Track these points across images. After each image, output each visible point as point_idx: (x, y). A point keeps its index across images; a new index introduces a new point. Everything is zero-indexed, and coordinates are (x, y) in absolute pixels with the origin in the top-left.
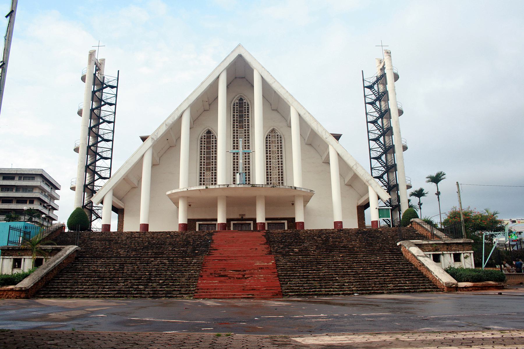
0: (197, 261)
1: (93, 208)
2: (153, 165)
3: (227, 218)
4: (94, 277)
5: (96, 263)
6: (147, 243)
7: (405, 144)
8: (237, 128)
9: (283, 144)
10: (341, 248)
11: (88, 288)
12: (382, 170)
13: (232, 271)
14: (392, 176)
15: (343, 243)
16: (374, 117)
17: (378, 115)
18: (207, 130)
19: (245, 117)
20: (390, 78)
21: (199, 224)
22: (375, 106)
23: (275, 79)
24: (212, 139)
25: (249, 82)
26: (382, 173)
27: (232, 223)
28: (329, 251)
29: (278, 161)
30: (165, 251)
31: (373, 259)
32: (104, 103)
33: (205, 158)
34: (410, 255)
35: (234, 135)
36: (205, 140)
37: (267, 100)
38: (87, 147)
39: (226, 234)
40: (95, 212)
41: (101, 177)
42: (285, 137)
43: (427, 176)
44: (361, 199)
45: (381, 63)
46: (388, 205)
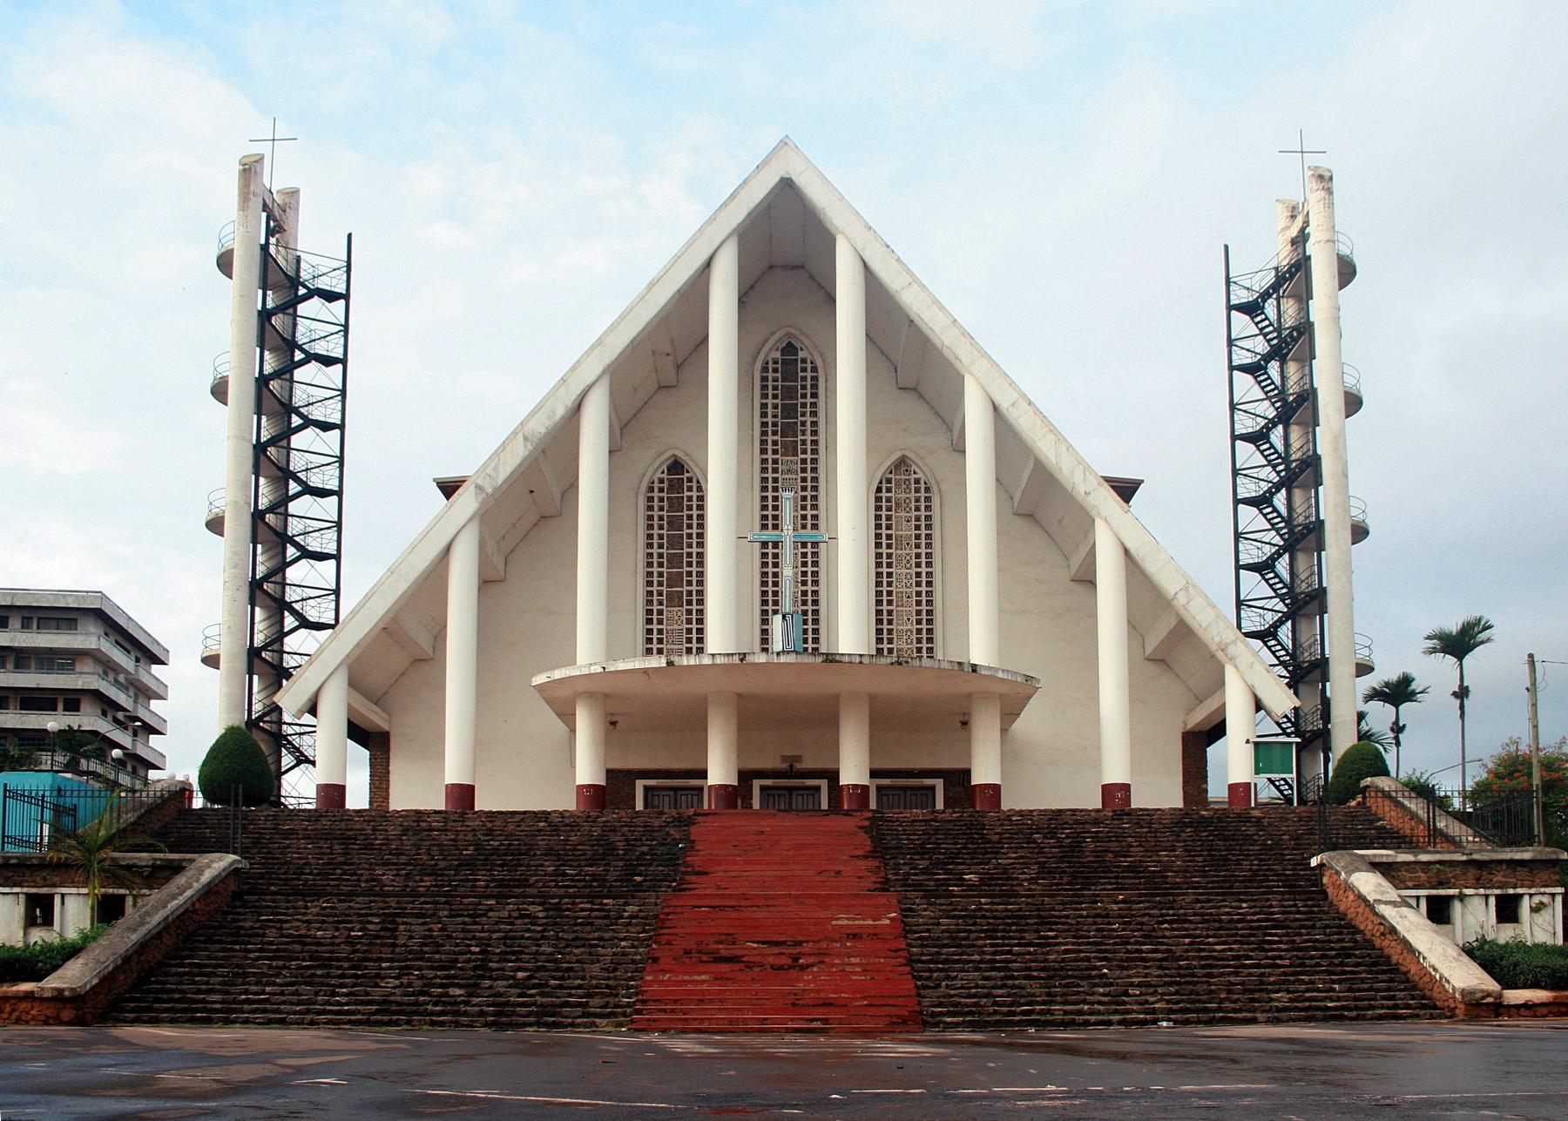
0: (640, 911)
1: (284, 727)
2: (485, 582)
5: (304, 914)
6: (472, 848)
7: (1361, 517)
8: (775, 452)
10: (1123, 872)
11: (282, 993)
12: (1273, 542)
14: (1308, 632)
16: (1259, 419)
17: (1271, 413)
18: (668, 459)
21: (647, 789)
23: (912, 274)
27: (757, 784)
29: (918, 575)
31: (1227, 910)
33: (665, 560)
35: (764, 480)
36: (665, 495)
39: (737, 823)
41: (305, 623)
42: (944, 487)
43: (1429, 632)
45: (1293, 217)
46: (1288, 731)
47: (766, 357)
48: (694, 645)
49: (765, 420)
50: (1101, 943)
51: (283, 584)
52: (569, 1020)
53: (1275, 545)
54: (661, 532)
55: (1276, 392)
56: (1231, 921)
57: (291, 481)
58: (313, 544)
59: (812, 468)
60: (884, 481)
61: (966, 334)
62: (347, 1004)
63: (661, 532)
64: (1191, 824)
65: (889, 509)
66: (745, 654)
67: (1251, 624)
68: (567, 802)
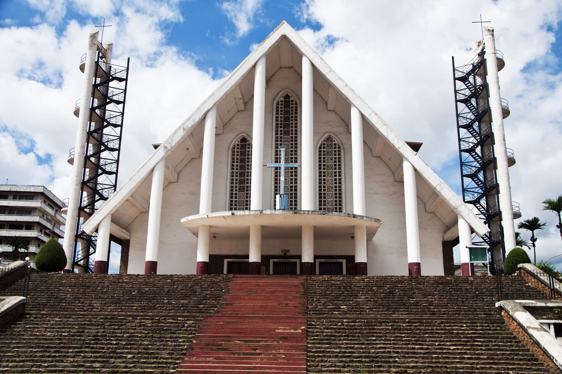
0: (193, 323)
2: (170, 182)
6: (136, 291)
7: (512, 156)
10: (411, 306)
11: (16, 366)
12: (476, 166)
13: (239, 342)
15: (414, 298)
16: (468, 120)
17: (473, 117)
18: (241, 136)
19: (292, 120)
22: (470, 105)
24: (247, 150)
26: (479, 196)
28: (393, 311)
29: (336, 179)
30: (157, 304)
38: (85, 158)
39: (249, 281)
42: (345, 146)
43: (544, 201)
44: (448, 232)
45: (479, 46)
46: (487, 240)
48: (293, 207)
49: (277, 122)
50: (396, 344)
53: (477, 167)
54: (237, 164)
55: (475, 109)
56: (458, 333)
58: (108, 168)
59: (295, 140)
60: (322, 145)
61: (351, 89)
63: (237, 164)
67: (469, 198)
68: (192, 271)
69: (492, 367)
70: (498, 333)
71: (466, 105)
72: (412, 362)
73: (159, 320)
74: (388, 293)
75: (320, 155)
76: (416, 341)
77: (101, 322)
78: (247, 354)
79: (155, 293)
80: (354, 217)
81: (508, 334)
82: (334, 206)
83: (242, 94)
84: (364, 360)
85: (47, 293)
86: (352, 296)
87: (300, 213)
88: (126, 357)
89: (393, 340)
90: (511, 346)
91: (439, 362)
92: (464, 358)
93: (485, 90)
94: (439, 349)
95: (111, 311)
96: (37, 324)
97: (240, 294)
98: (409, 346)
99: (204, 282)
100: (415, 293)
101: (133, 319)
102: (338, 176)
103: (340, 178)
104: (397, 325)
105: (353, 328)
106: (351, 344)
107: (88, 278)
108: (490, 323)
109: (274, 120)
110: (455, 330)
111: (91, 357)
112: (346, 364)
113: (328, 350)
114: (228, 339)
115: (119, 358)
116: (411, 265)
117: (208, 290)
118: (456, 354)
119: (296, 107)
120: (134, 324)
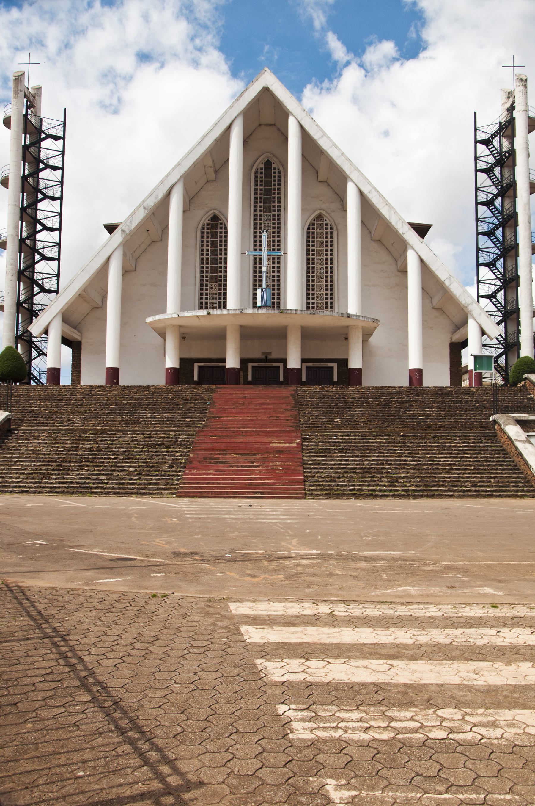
0: (186, 438)
1: (33, 338)
2: (126, 271)
3: (243, 357)
4: (34, 461)
8: (261, 211)
9: (335, 239)
10: (407, 419)
11: (27, 478)
12: (496, 252)
13: (235, 456)
16: (489, 195)
17: (495, 192)
19: (274, 194)
20: (521, 126)
21: (199, 367)
23: (323, 132)
24: (220, 230)
25: (282, 133)
27: (250, 365)
29: (327, 268)
32: (44, 166)
33: (209, 261)
34: (506, 437)
35: (255, 224)
36: (209, 231)
37: (311, 165)
38: (20, 240)
39: (235, 392)
40: (35, 345)
41: (43, 290)
42: (339, 227)
44: (457, 332)
45: (508, 98)
46: (502, 342)
47: (257, 167)
50: (390, 456)
51: (33, 272)
52: (151, 492)
56: (450, 446)
57: (38, 225)
61: (348, 159)
62: (55, 483)
64: (441, 395)
65: (313, 237)
66: (242, 309)
67: (484, 291)
68: (160, 381)
69: (476, 477)
70: (488, 446)
71: (488, 175)
72: (403, 473)
73: (150, 434)
74: (385, 405)
75: (308, 237)
76: (409, 453)
77: (92, 437)
78: (246, 466)
79: (134, 406)
80: (348, 317)
81: (497, 446)
82: (325, 301)
83: (213, 161)
84: (358, 471)
85: (19, 407)
86: (346, 408)
87: (286, 313)
88: (128, 471)
89: (387, 453)
90: (498, 457)
91: (428, 473)
92: (452, 469)
93: (511, 158)
94: (429, 461)
95: (93, 426)
96: (29, 440)
97: (226, 407)
98: (402, 459)
99: (186, 393)
100: (412, 406)
101: (124, 434)
102: (329, 263)
103: (332, 266)
104: (392, 439)
105: (348, 442)
106: (345, 457)
107: (56, 391)
108: (483, 436)
109: (253, 193)
110: (447, 443)
111: (94, 470)
112: (341, 475)
113: (323, 462)
114: (224, 452)
115: (121, 471)
116: (412, 371)
117: (191, 403)
118: (445, 465)
119: (280, 177)
120: (126, 439)
